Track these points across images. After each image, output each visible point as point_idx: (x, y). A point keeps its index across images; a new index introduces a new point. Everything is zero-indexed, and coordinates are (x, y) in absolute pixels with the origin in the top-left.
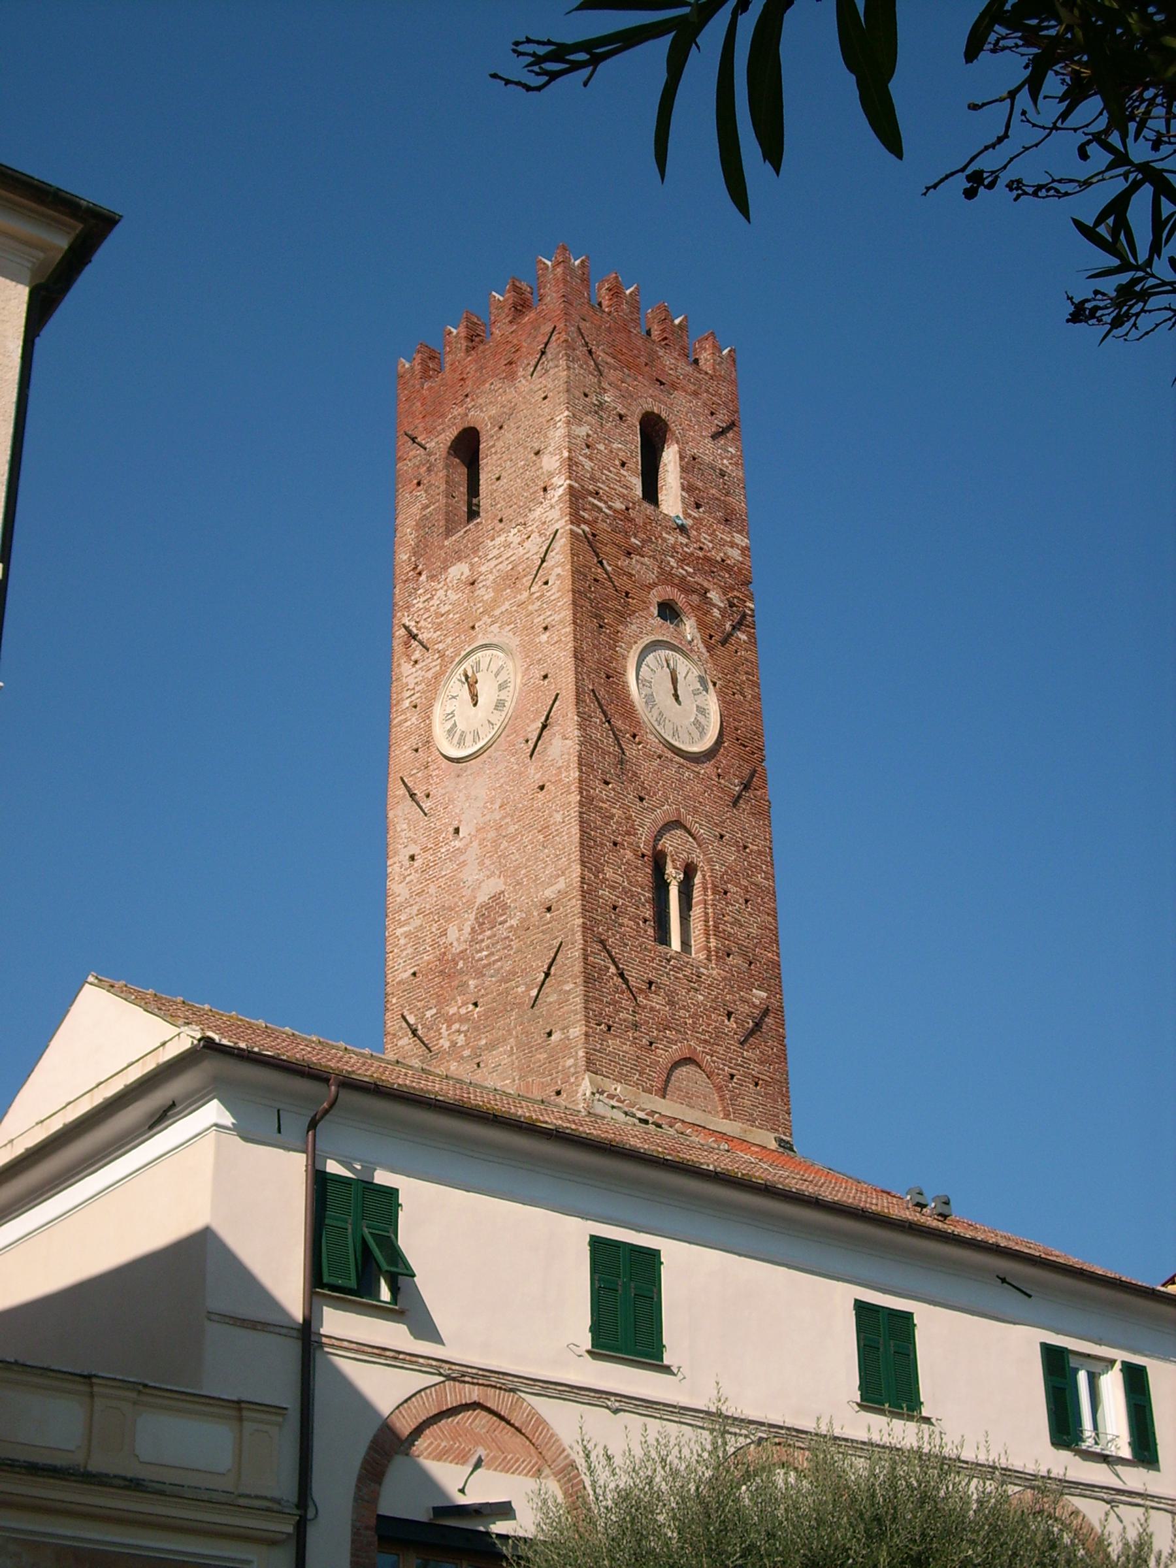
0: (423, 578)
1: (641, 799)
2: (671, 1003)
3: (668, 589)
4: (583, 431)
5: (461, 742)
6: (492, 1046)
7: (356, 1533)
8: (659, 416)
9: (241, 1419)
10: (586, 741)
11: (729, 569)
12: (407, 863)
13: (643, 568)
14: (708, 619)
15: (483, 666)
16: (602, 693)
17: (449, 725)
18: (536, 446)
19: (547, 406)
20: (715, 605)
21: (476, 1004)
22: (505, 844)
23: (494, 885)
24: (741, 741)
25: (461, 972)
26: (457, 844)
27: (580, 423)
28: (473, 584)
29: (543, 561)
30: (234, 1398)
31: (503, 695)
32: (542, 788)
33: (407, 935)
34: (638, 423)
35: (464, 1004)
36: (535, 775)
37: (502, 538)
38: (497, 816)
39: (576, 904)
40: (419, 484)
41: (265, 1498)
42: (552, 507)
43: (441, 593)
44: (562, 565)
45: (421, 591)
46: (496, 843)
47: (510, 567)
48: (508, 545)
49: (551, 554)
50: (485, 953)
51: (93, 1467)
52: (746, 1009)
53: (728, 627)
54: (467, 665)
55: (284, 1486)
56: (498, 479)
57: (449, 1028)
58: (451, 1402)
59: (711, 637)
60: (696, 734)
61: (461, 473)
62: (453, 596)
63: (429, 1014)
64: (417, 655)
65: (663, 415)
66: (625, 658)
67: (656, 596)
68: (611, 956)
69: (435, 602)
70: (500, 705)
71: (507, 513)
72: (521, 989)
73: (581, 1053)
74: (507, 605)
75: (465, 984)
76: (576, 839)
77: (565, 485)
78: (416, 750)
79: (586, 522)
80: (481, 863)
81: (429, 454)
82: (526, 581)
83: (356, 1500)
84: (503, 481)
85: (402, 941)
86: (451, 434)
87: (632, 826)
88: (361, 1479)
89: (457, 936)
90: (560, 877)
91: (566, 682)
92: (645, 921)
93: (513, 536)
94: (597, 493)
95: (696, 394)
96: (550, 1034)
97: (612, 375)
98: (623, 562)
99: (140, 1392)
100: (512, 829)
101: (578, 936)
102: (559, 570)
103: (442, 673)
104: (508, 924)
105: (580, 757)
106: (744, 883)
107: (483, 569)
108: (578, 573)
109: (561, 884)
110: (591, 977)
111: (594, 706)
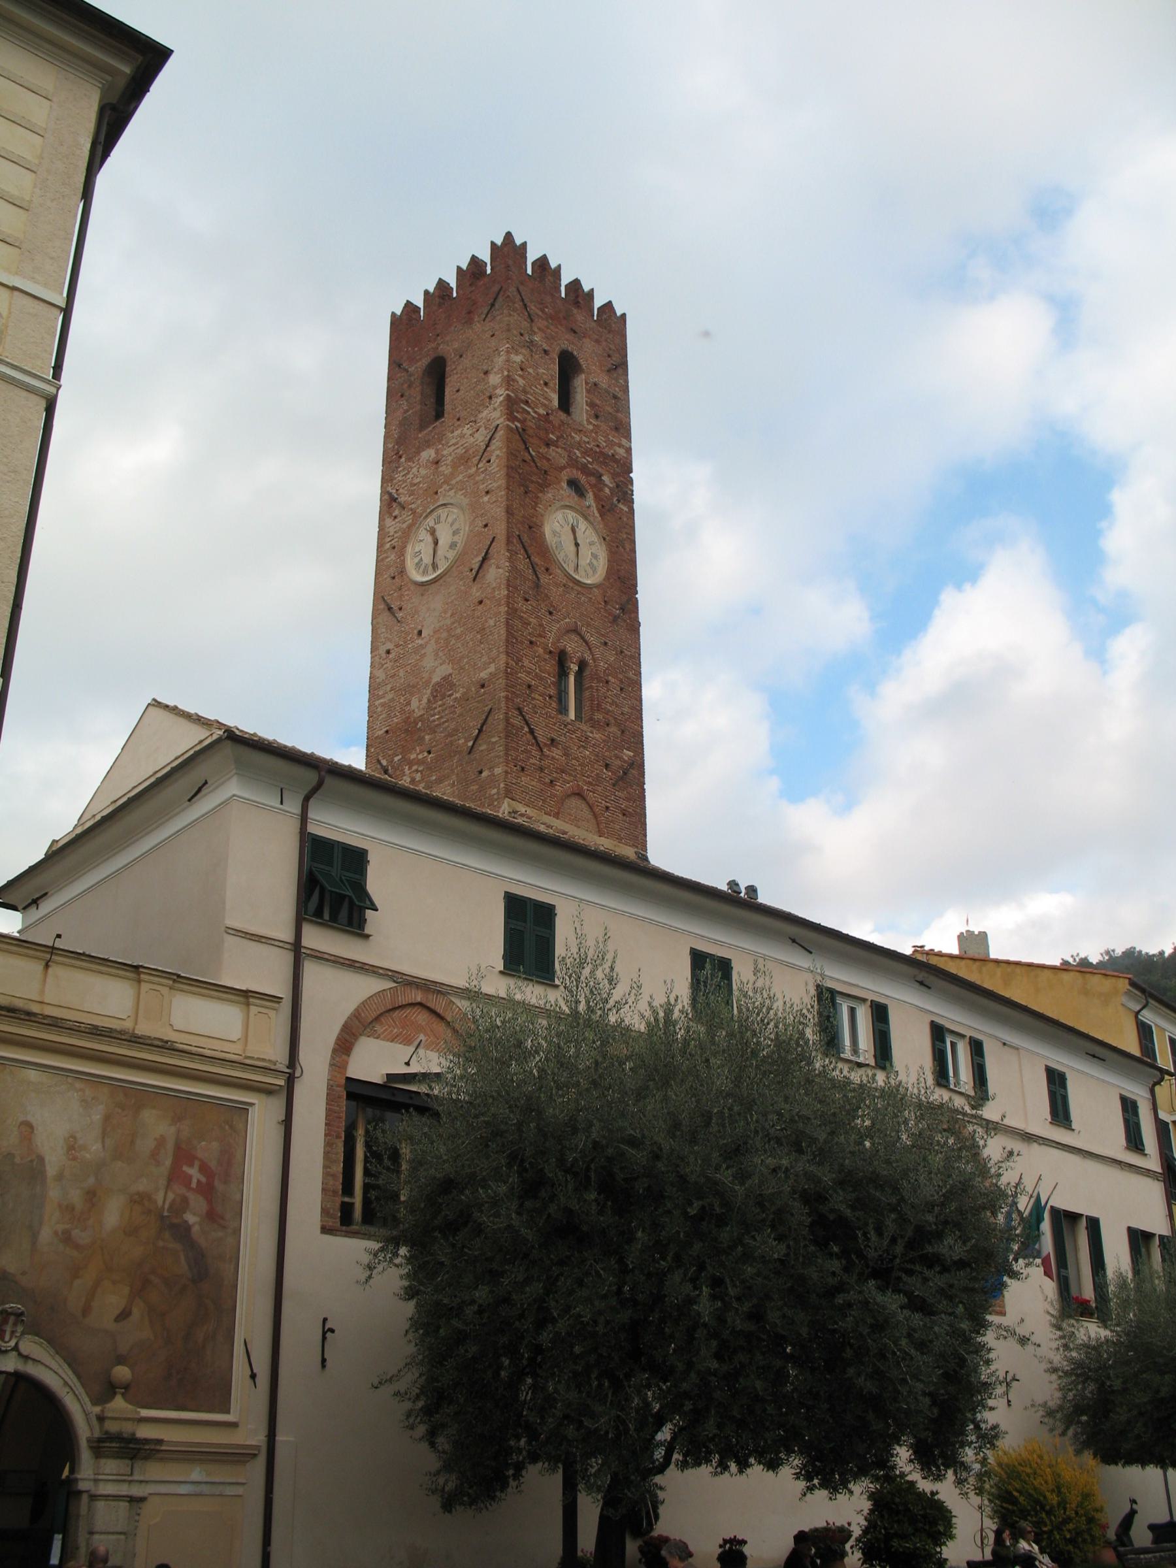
0: (403, 460)
1: (551, 613)
2: (566, 755)
4: (518, 359)
5: (425, 572)
7: (330, 1088)
8: (572, 354)
9: (248, 1004)
10: (514, 569)
11: (617, 461)
12: (384, 655)
13: (557, 455)
14: (601, 494)
15: (443, 518)
16: (525, 538)
17: (416, 560)
18: (485, 368)
19: (493, 343)
21: (429, 752)
22: (453, 642)
23: (445, 670)
25: (420, 729)
26: (420, 642)
27: (517, 353)
28: (437, 463)
29: (487, 446)
30: (244, 988)
31: (456, 538)
32: (481, 602)
33: (383, 705)
35: (421, 752)
36: (476, 593)
37: (459, 432)
38: (448, 622)
39: (502, 682)
40: (402, 396)
41: (263, 1060)
42: (495, 409)
43: (415, 470)
44: (500, 449)
48: (462, 436)
51: (139, 1031)
52: (618, 762)
54: (430, 521)
55: (276, 1053)
58: (402, 1000)
60: (590, 572)
62: (423, 472)
63: (396, 759)
64: (396, 513)
67: (565, 475)
68: (525, 720)
69: (410, 476)
70: (453, 545)
72: (461, 741)
73: (502, 785)
74: (460, 477)
76: (504, 637)
79: (519, 420)
80: (437, 654)
81: (411, 375)
82: (475, 460)
83: (331, 1065)
84: (461, 392)
85: (379, 709)
86: (425, 362)
88: (334, 1051)
89: (417, 705)
90: (490, 665)
91: (500, 529)
92: (550, 697)
93: (467, 430)
95: (597, 341)
96: (481, 772)
97: (541, 323)
98: (543, 450)
99: (174, 981)
100: (459, 631)
101: (503, 705)
102: (498, 452)
105: (508, 580)
106: (621, 676)
107: (445, 452)
108: (511, 454)
109: (492, 669)
110: (510, 733)
111: (519, 546)
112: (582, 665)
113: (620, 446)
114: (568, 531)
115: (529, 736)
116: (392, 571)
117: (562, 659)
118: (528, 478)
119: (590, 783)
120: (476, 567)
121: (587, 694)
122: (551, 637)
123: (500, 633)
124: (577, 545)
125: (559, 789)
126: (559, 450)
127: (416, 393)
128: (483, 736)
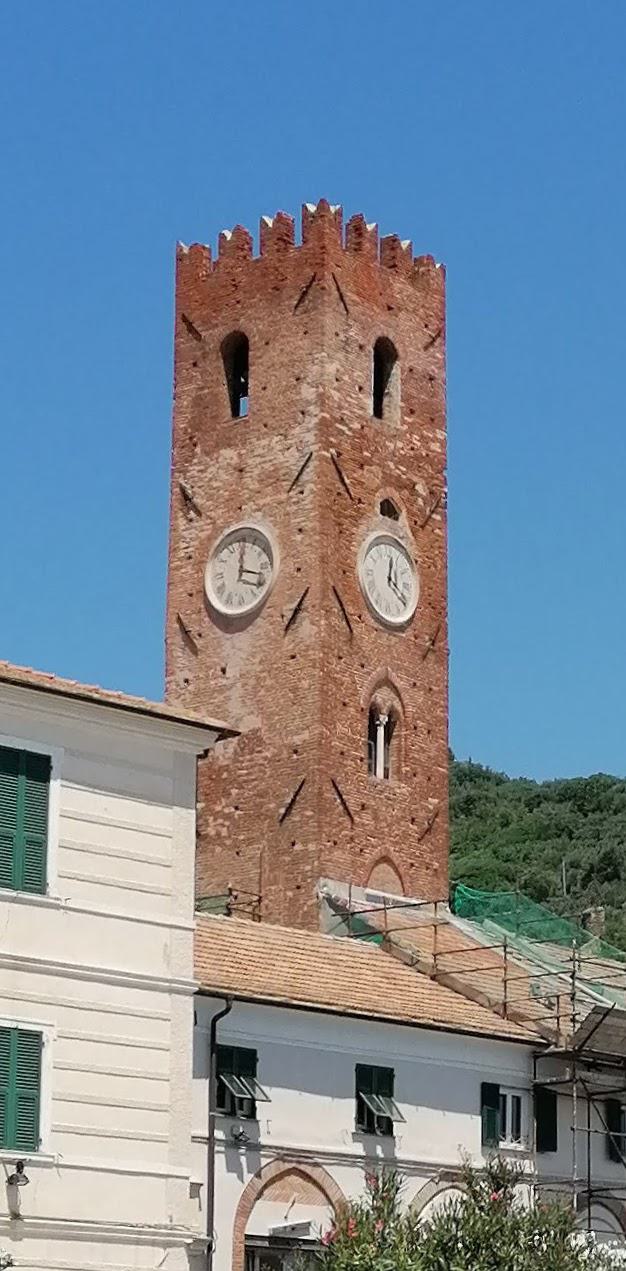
1: (363, 666)
3: (388, 489)
5: (228, 602)
6: (250, 842)
20: (419, 496)
22: (262, 692)
24: (434, 604)
28: (241, 471)
34: (372, 350)
36: (288, 645)
45: (195, 461)
46: (256, 692)
47: (272, 468)
50: (245, 772)
53: (428, 512)
56: (264, 388)
57: (215, 820)
59: (416, 522)
65: (391, 337)
66: (356, 554)
67: (378, 499)
77: (320, 417)
78: (191, 595)
79: (332, 445)
82: (286, 485)
87: (356, 689)
94: (342, 419)
96: (293, 844)
104: (263, 755)
109: (306, 735)
113: (435, 440)
117: (373, 713)
118: (340, 515)
120: (289, 615)
123: (312, 698)
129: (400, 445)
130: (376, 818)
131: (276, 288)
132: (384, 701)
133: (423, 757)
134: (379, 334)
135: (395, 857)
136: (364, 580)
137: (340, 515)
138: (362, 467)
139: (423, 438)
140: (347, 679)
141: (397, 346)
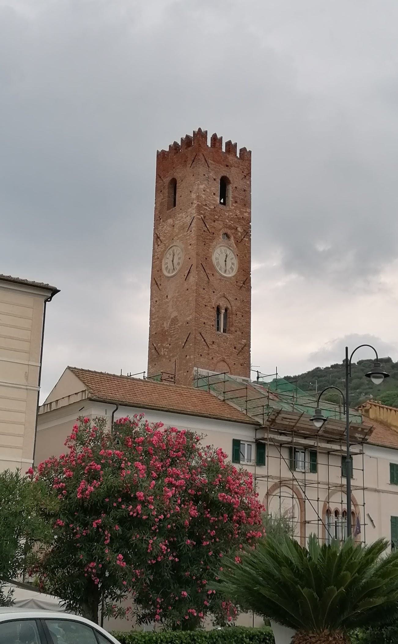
1: (214, 292)
5: (169, 272)
6: (173, 356)
16: (204, 265)
23: (175, 314)
33: (154, 322)
36: (186, 286)
38: (177, 295)
49: (193, 223)
60: (231, 271)
61: (172, 191)
62: (169, 229)
67: (221, 233)
70: (178, 264)
71: (183, 208)
75: (168, 339)
79: (202, 214)
84: (182, 198)
91: (194, 262)
93: (184, 215)
95: (238, 167)
98: (213, 224)
103: (165, 250)
109: (191, 317)
112: (226, 310)
113: (246, 212)
114: (223, 257)
115: (204, 343)
116: (158, 268)
117: (218, 309)
118: (206, 238)
119: (228, 356)
120: (186, 275)
121: (228, 320)
122: (213, 302)
123: (193, 304)
124: (226, 261)
125: (215, 360)
126: (219, 222)
127: (166, 191)
128: (187, 343)
129: (231, 214)
130: (219, 346)
131: (185, 161)
132: (223, 305)
133: (240, 325)
134: (222, 175)
135: (228, 361)
136: (215, 262)
137: (206, 238)
138: (214, 221)
139: (241, 212)
140: (207, 297)
141: (230, 179)
